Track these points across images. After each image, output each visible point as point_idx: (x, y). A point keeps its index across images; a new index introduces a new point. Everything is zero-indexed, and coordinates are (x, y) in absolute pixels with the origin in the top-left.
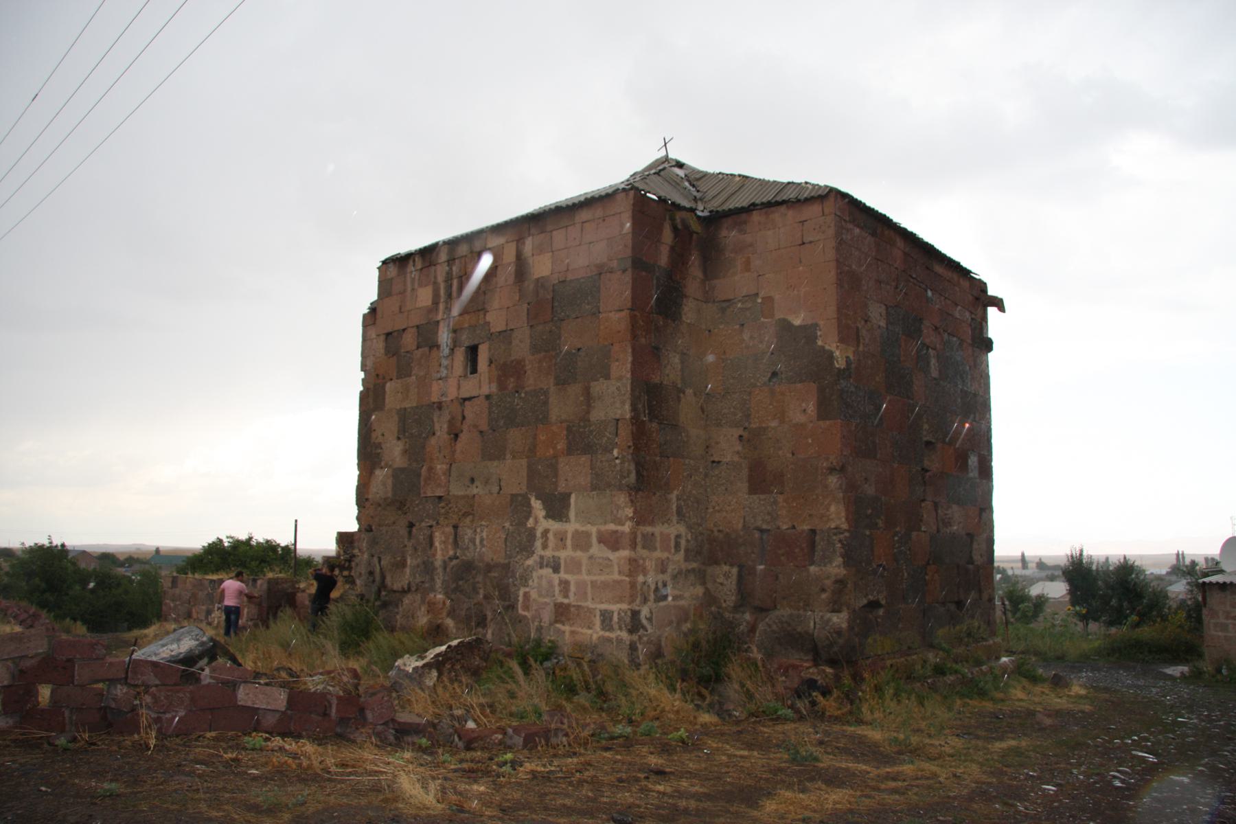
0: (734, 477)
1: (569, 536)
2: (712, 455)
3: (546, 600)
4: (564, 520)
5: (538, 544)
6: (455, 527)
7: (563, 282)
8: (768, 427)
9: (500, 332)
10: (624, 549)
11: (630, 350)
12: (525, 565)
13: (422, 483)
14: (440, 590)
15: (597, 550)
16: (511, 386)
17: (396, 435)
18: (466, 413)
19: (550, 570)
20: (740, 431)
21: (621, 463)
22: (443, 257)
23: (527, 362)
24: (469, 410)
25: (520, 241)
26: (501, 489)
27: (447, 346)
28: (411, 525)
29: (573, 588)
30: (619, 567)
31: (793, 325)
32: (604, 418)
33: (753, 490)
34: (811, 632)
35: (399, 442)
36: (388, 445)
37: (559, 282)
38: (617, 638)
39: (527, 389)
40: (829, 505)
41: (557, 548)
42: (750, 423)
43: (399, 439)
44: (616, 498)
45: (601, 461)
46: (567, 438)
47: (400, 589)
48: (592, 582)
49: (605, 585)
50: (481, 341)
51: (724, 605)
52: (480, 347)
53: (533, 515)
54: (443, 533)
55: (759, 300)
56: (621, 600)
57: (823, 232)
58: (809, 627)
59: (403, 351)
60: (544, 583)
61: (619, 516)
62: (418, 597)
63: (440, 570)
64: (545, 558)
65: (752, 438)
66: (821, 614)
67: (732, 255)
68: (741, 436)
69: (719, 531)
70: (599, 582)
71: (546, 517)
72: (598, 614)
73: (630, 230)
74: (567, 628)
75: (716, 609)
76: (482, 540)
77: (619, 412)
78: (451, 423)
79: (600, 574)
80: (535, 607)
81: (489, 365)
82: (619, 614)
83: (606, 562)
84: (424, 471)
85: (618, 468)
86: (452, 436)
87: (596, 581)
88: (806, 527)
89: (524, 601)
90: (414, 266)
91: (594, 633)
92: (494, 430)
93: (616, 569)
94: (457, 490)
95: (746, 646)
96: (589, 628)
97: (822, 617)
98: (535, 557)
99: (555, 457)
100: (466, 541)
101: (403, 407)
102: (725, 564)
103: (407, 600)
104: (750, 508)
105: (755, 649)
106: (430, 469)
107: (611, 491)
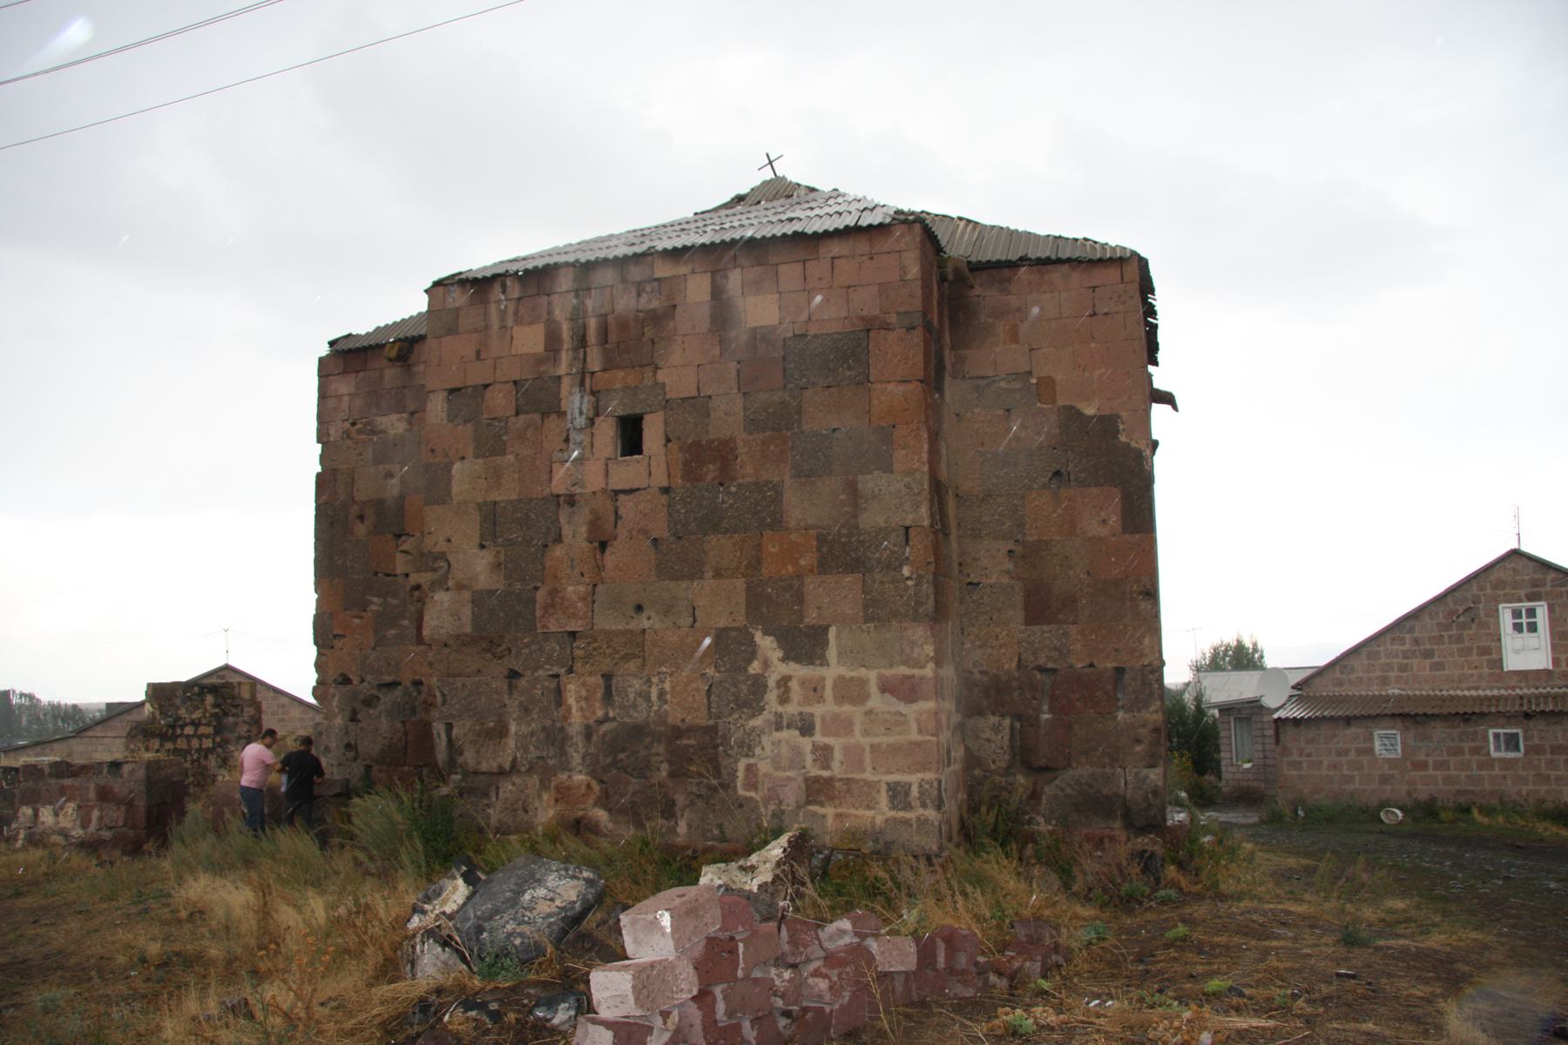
0: (1003, 602)
1: (829, 684)
2: (969, 575)
3: (788, 774)
4: (818, 662)
5: (772, 696)
6: (608, 677)
7: (804, 335)
8: (1051, 540)
9: (683, 399)
10: (926, 699)
11: (926, 436)
12: (747, 728)
13: (538, 613)
14: (580, 768)
15: (876, 701)
16: (710, 476)
17: (477, 540)
18: (622, 511)
19: (797, 733)
20: (1011, 546)
21: (916, 585)
22: (565, 283)
23: (740, 443)
24: (627, 505)
25: (717, 274)
26: (695, 621)
27: (581, 413)
28: (513, 675)
29: (838, 756)
30: (919, 724)
31: (1083, 415)
32: (883, 525)
33: (1030, 620)
34: (1122, 793)
35: (485, 552)
36: (461, 556)
37: (795, 336)
38: (918, 819)
39: (741, 481)
40: (1143, 637)
41: (807, 701)
42: (1024, 535)
43: (482, 547)
44: (909, 632)
45: (882, 583)
46: (819, 550)
47: (495, 770)
48: (872, 746)
49: (895, 749)
50: (648, 409)
51: (993, 767)
52: (645, 417)
53: (759, 657)
54: (584, 684)
55: (1034, 381)
56: (924, 767)
57: (1124, 303)
58: (1119, 787)
59: (485, 416)
60: (785, 750)
61: (915, 655)
62: (535, 779)
63: (579, 740)
64: (785, 716)
65: (1028, 555)
66: (1135, 770)
67: (990, 320)
68: (1010, 551)
69: (982, 672)
70: (884, 746)
71: (783, 660)
72: (884, 788)
73: (919, 276)
74: (829, 811)
75: (982, 773)
76: (662, 694)
77: (911, 517)
78: (595, 525)
79: (885, 735)
80: (767, 785)
81: (666, 445)
82: (920, 786)
83: (897, 717)
84: (541, 596)
85: (911, 592)
86: (596, 544)
87: (879, 745)
88: (1110, 665)
89: (746, 778)
90: (504, 292)
91: (881, 813)
92: (680, 538)
93: (914, 726)
94: (607, 622)
95: (1027, 817)
96: (868, 807)
97: (1137, 774)
98: (766, 715)
99: (799, 576)
100: (631, 696)
101: (490, 498)
102: (993, 714)
103: (507, 788)
104: (1028, 642)
105: (1041, 820)
106: (553, 593)
107: (901, 622)
